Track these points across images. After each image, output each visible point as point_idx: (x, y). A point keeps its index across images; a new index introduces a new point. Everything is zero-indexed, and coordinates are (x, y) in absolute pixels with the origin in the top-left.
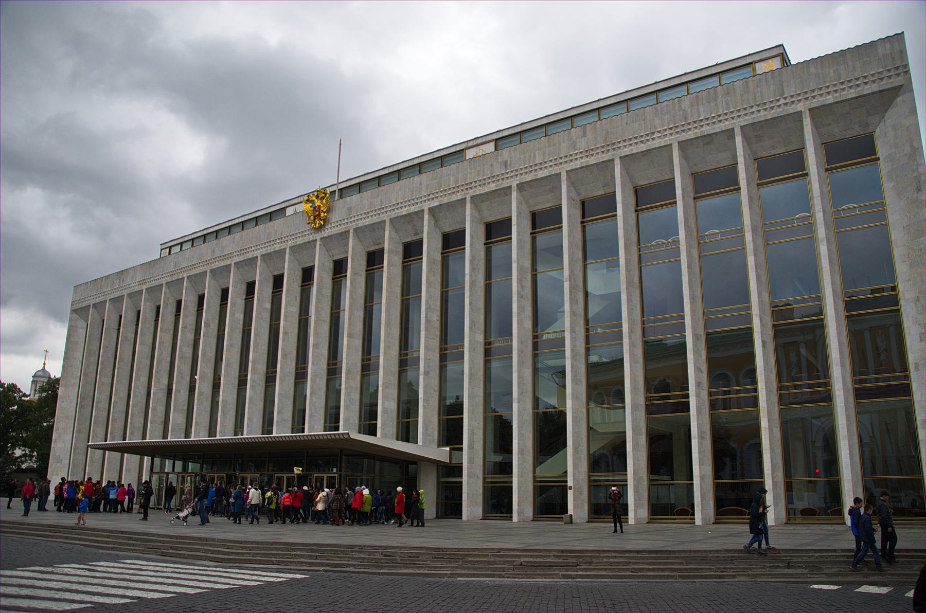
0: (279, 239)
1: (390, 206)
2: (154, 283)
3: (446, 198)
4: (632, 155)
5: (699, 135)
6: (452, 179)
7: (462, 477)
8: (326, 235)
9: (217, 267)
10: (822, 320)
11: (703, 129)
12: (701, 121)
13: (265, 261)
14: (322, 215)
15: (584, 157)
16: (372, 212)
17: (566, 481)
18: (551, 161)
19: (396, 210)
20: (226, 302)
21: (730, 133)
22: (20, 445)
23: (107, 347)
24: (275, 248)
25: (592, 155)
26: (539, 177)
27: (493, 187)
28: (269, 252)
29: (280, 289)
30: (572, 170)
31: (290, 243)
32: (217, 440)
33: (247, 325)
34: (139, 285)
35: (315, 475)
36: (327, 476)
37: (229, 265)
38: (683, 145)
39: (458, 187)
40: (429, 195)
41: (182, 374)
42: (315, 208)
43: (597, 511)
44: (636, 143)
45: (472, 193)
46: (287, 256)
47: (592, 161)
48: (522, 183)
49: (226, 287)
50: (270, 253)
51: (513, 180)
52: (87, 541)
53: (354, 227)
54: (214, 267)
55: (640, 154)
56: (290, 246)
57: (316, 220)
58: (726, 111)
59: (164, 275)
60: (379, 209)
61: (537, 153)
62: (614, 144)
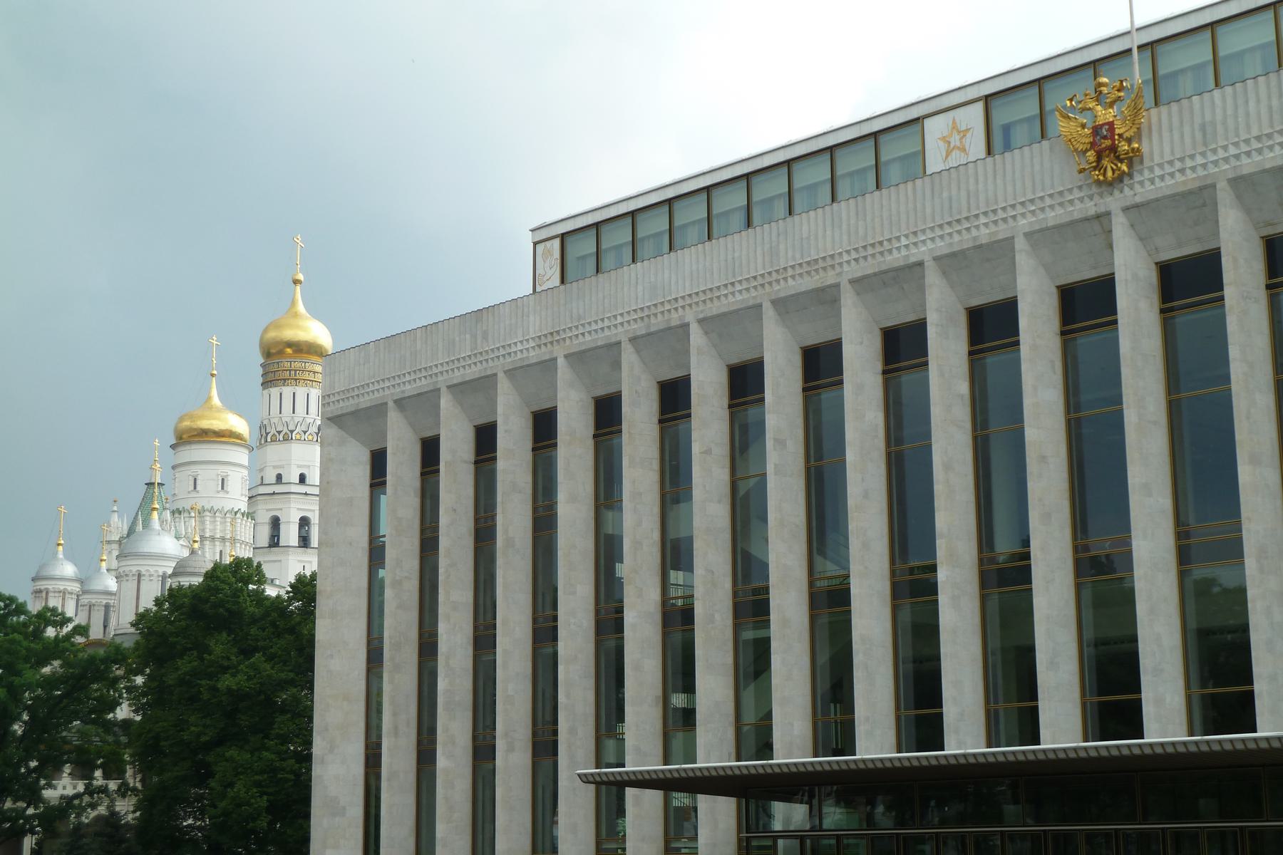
2: (588, 341)
8: (1138, 199)
24: (975, 238)
28: (956, 248)
29: (684, 412)
33: (482, 511)
37: (830, 286)
41: (713, 572)
42: (1096, 130)
49: (911, 318)
57: (1105, 162)
59: (620, 319)
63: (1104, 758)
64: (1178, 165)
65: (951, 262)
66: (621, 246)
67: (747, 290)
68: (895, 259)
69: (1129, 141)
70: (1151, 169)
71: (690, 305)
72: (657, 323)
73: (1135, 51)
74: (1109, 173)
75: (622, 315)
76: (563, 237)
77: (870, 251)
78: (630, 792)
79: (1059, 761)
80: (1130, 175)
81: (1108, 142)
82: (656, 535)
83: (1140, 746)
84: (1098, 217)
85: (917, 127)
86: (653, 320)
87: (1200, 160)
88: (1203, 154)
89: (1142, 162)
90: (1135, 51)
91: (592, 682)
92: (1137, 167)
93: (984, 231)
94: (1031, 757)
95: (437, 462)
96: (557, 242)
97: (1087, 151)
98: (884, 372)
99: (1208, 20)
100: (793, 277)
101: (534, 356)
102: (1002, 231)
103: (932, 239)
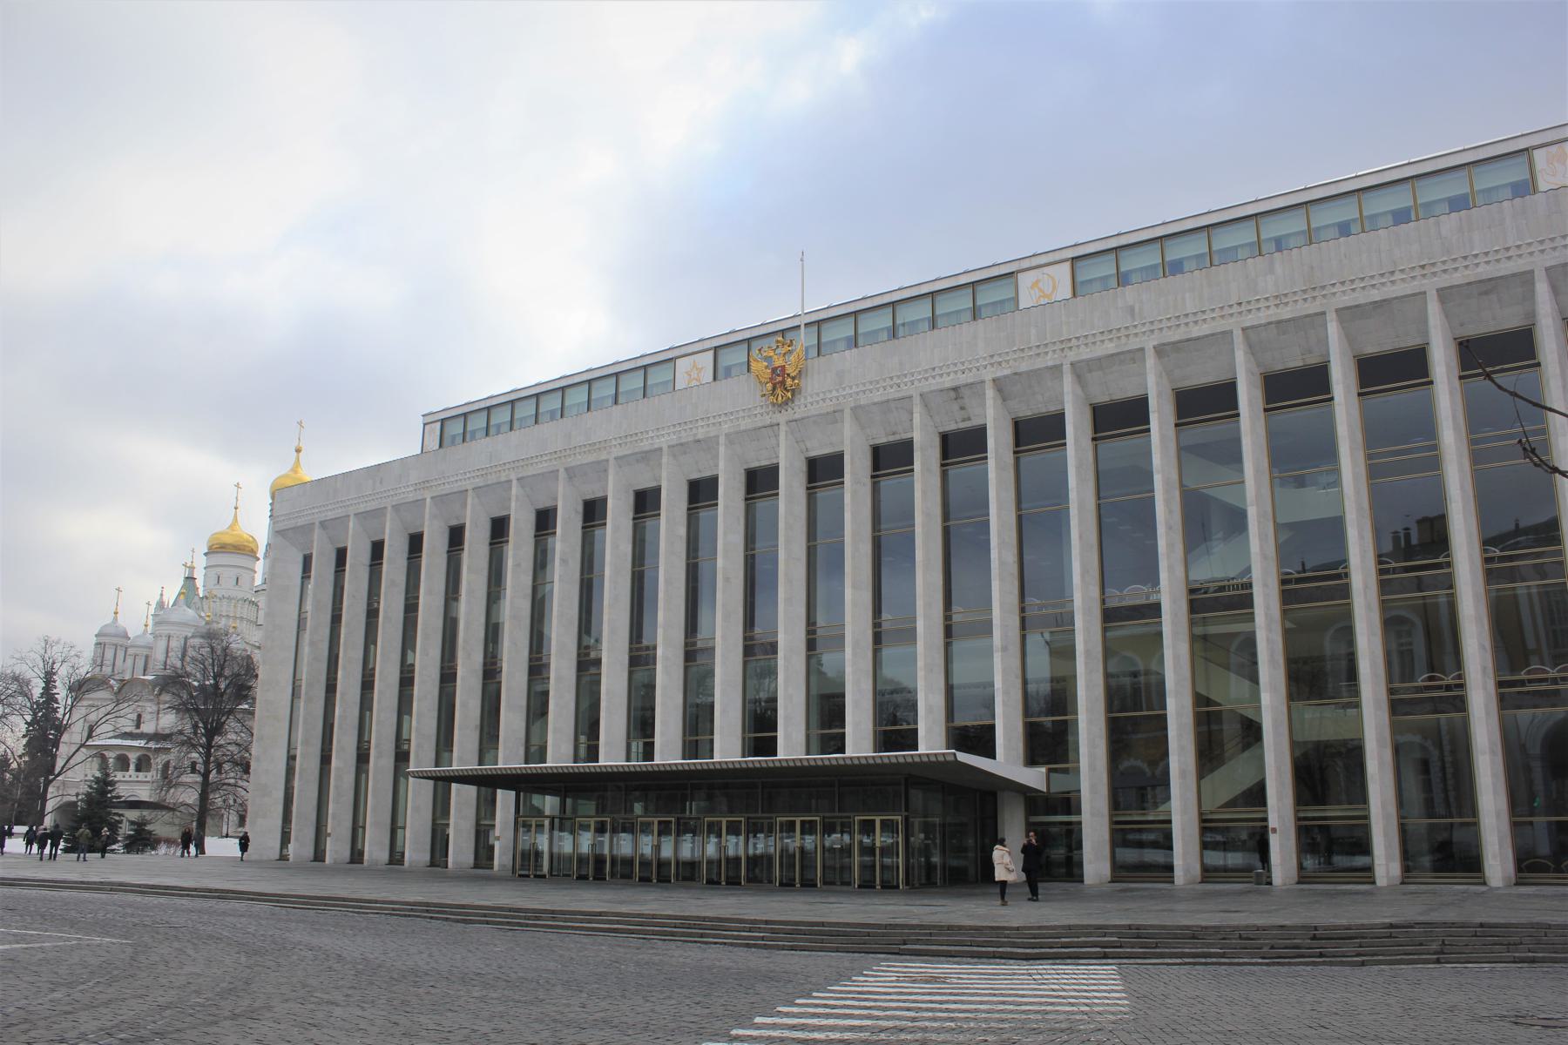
0: (702, 419)
1: (919, 373)
2: (447, 489)
3: (1024, 364)
4: (1357, 306)
5: (1472, 279)
6: (1033, 331)
7: (1080, 814)
9: (579, 463)
10: (1349, 604)
11: (1480, 269)
12: (1476, 256)
13: (674, 456)
14: (789, 381)
15: (1273, 307)
16: (884, 380)
17: (1265, 820)
18: (1213, 310)
19: (937, 377)
20: (658, 512)
21: (1526, 278)
22: (13, 781)
23: (354, 596)
24: (695, 435)
25: (1286, 304)
26: (1194, 335)
27: (1110, 348)
30: (1253, 327)
31: (726, 427)
32: (453, 770)
34: (415, 490)
35: (706, 819)
36: (727, 821)
38: (1444, 294)
39: (1046, 345)
40: (992, 356)
42: (774, 370)
43: (1122, 872)
44: (1363, 288)
45: (1072, 356)
46: (722, 449)
47: (1286, 313)
48: (1164, 344)
50: (687, 443)
51: (1146, 338)
52: (578, 927)
53: (853, 405)
54: (573, 464)
55: (1371, 306)
56: (727, 432)
57: (779, 391)
58: (1519, 243)
59: (468, 475)
60: (898, 377)
61: (1187, 295)
62: (1323, 287)
63: (656, 771)
64: (822, 396)
65: (680, 449)
66: (668, 381)
67: (551, 460)
68: (645, 445)
69: (793, 378)
70: (806, 398)
71: (513, 468)
72: (492, 479)
73: (803, 327)
74: (780, 398)
75: (469, 472)
76: (443, 421)
77: (629, 439)
78: (454, 785)
79: (861, 765)
80: (793, 401)
81: (780, 379)
82: (483, 619)
83: (652, 765)
84: (771, 426)
85: (1012, 280)
86: (489, 477)
87: (835, 394)
88: (837, 391)
89: (800, 394)
90: (803, 327)
91: (435, 714)
92: (797, 396)
93: (700, 430)
94: (827, 763)
95: (420, 550)
96: (439, 424)
97: (767, 383)
98: (409, 559)
99: (1114, 245)
100: (580, 453)
101: (411, 497)
102: (713, 432)
103: (668, 434)
